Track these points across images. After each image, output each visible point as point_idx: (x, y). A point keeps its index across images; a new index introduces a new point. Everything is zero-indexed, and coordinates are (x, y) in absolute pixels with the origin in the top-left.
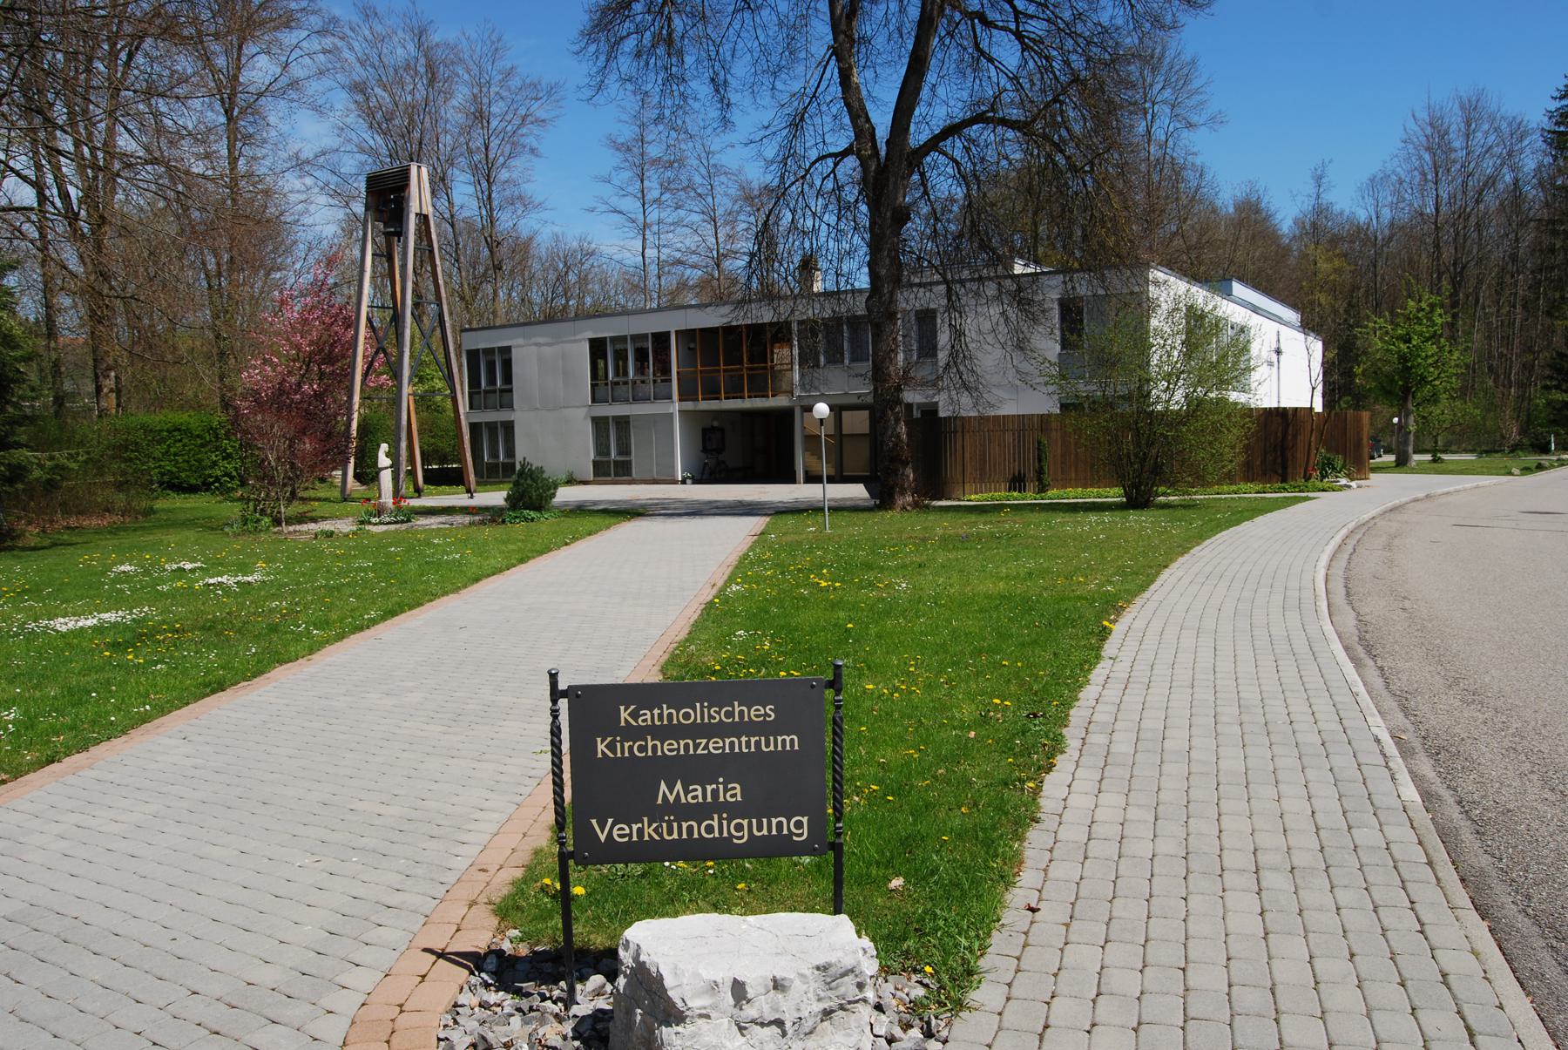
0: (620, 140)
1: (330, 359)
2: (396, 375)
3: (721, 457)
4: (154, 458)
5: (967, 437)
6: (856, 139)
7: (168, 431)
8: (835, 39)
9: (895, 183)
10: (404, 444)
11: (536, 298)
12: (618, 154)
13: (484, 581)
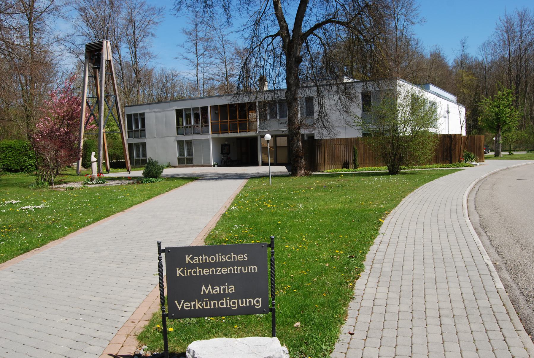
0: (187, 31)
1: (72, 118)
3: (229, 156)
5: (326, 146)
6: (280, 30)
7: (6, 148)
9: (296, 47)
10: (102, 152)
11: (154, 93)
12: (187, 36)
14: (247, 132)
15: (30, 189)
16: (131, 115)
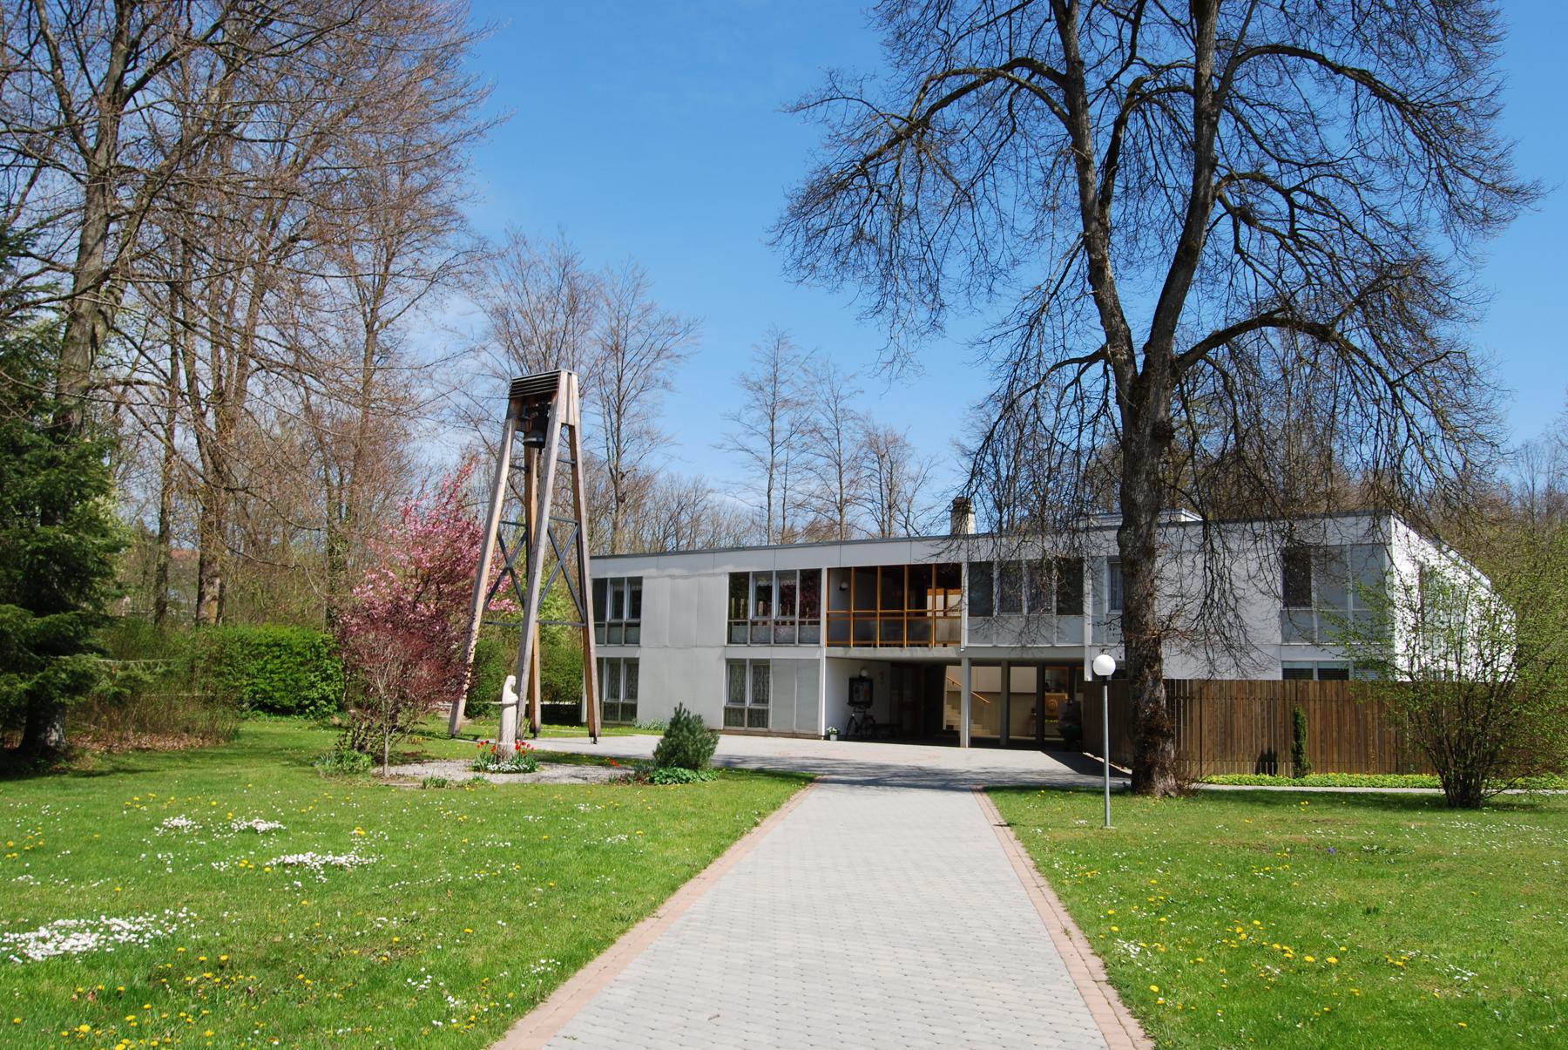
0: (754, 379)
1: (451, 578)
2: (525, 602)
4: (248, 675)
5: (1205, 703)
6: (1109, 341)
7: (267, 645)
8: (1086, 227)
9: (1157, 394)
10: (526, 678)
11: (647, 535)
12: (750, 392)
13: (684, 890)
14: (848, 646)
15: (317, 773)
16: (605, 580)
